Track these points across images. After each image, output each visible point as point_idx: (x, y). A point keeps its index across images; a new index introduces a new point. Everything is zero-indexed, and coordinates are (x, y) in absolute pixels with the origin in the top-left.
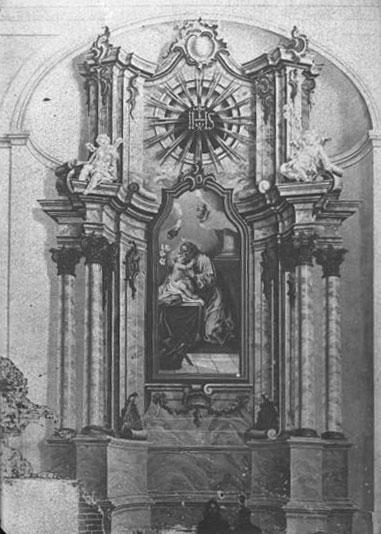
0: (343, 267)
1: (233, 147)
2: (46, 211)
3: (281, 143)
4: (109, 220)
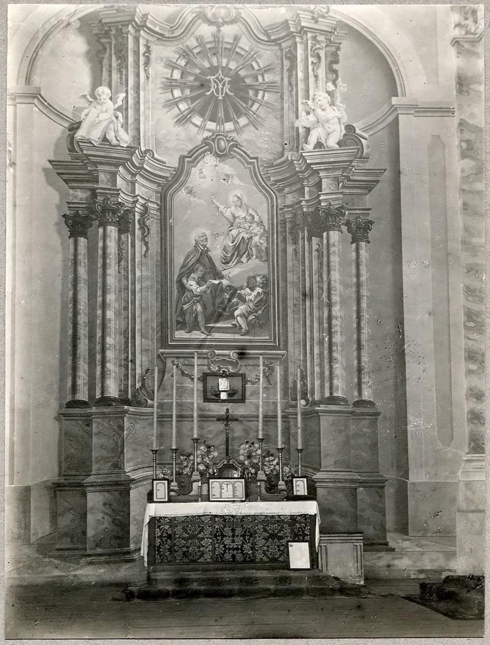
0: (371, 234)
1: (258, 112)
2: (59, 174)
3: (323, 352)
4: (124, 182)
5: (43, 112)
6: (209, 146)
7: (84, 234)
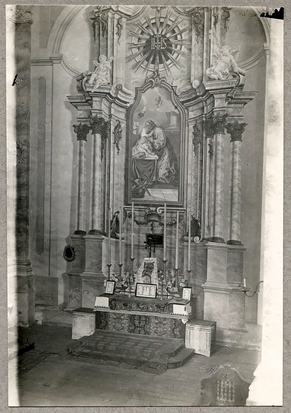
5: (67, 72)
6: (148, 84)
7: (85, 139)
